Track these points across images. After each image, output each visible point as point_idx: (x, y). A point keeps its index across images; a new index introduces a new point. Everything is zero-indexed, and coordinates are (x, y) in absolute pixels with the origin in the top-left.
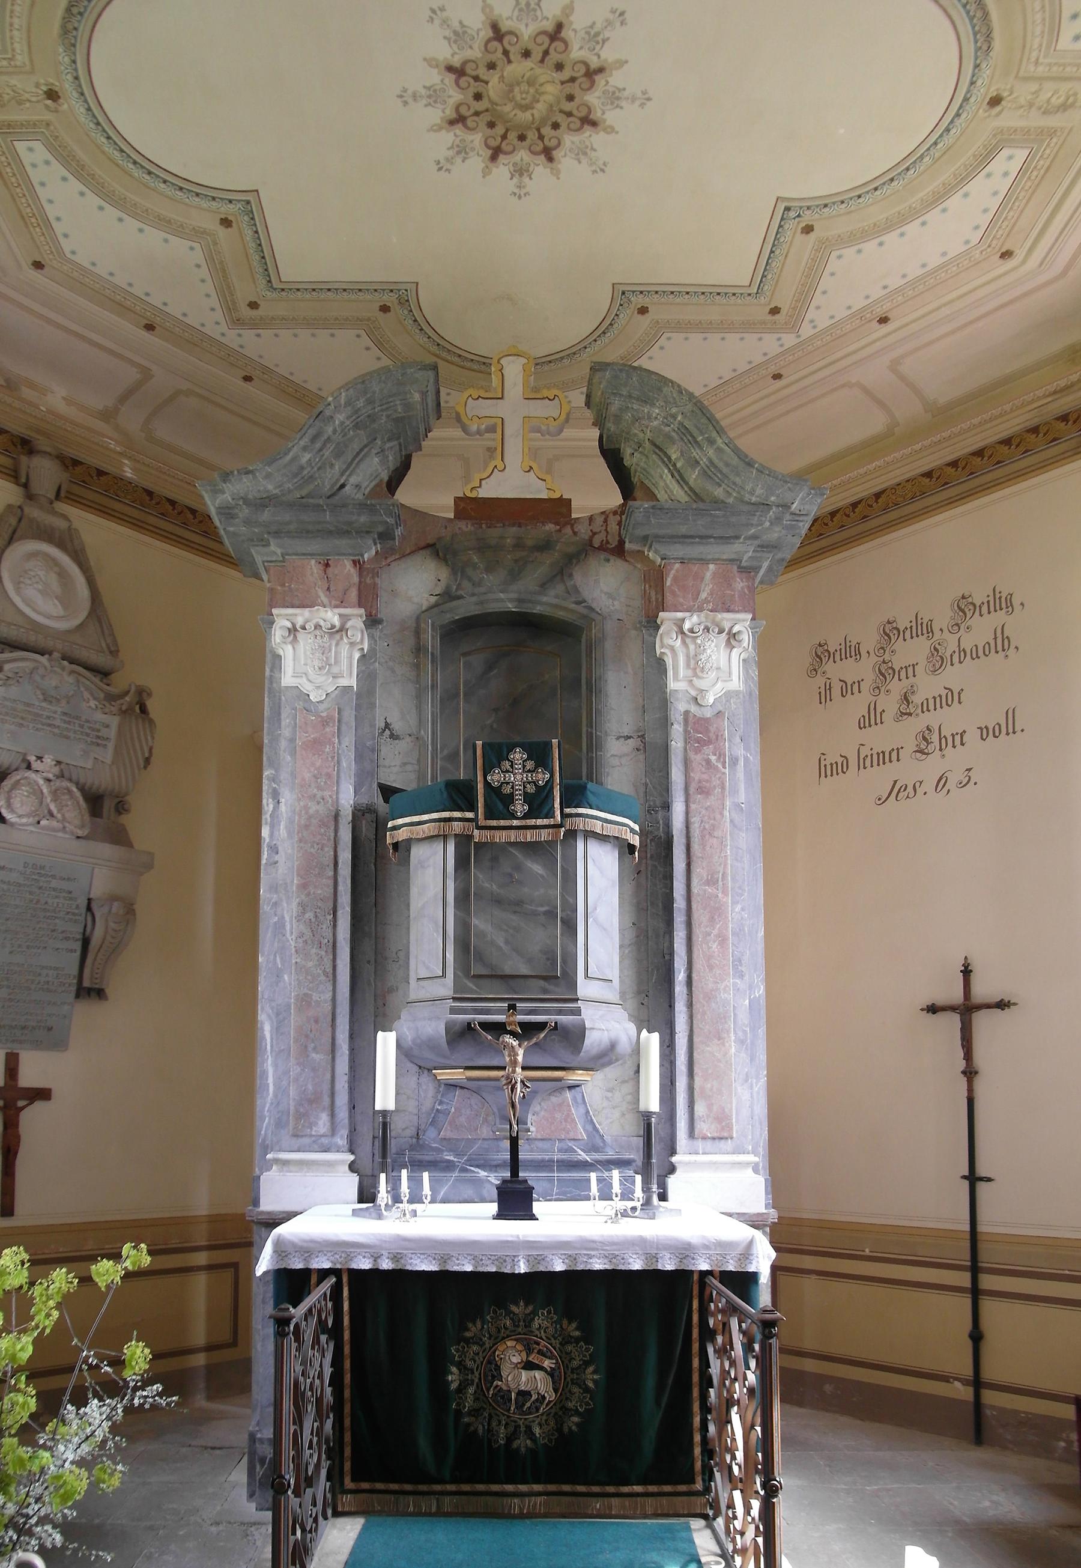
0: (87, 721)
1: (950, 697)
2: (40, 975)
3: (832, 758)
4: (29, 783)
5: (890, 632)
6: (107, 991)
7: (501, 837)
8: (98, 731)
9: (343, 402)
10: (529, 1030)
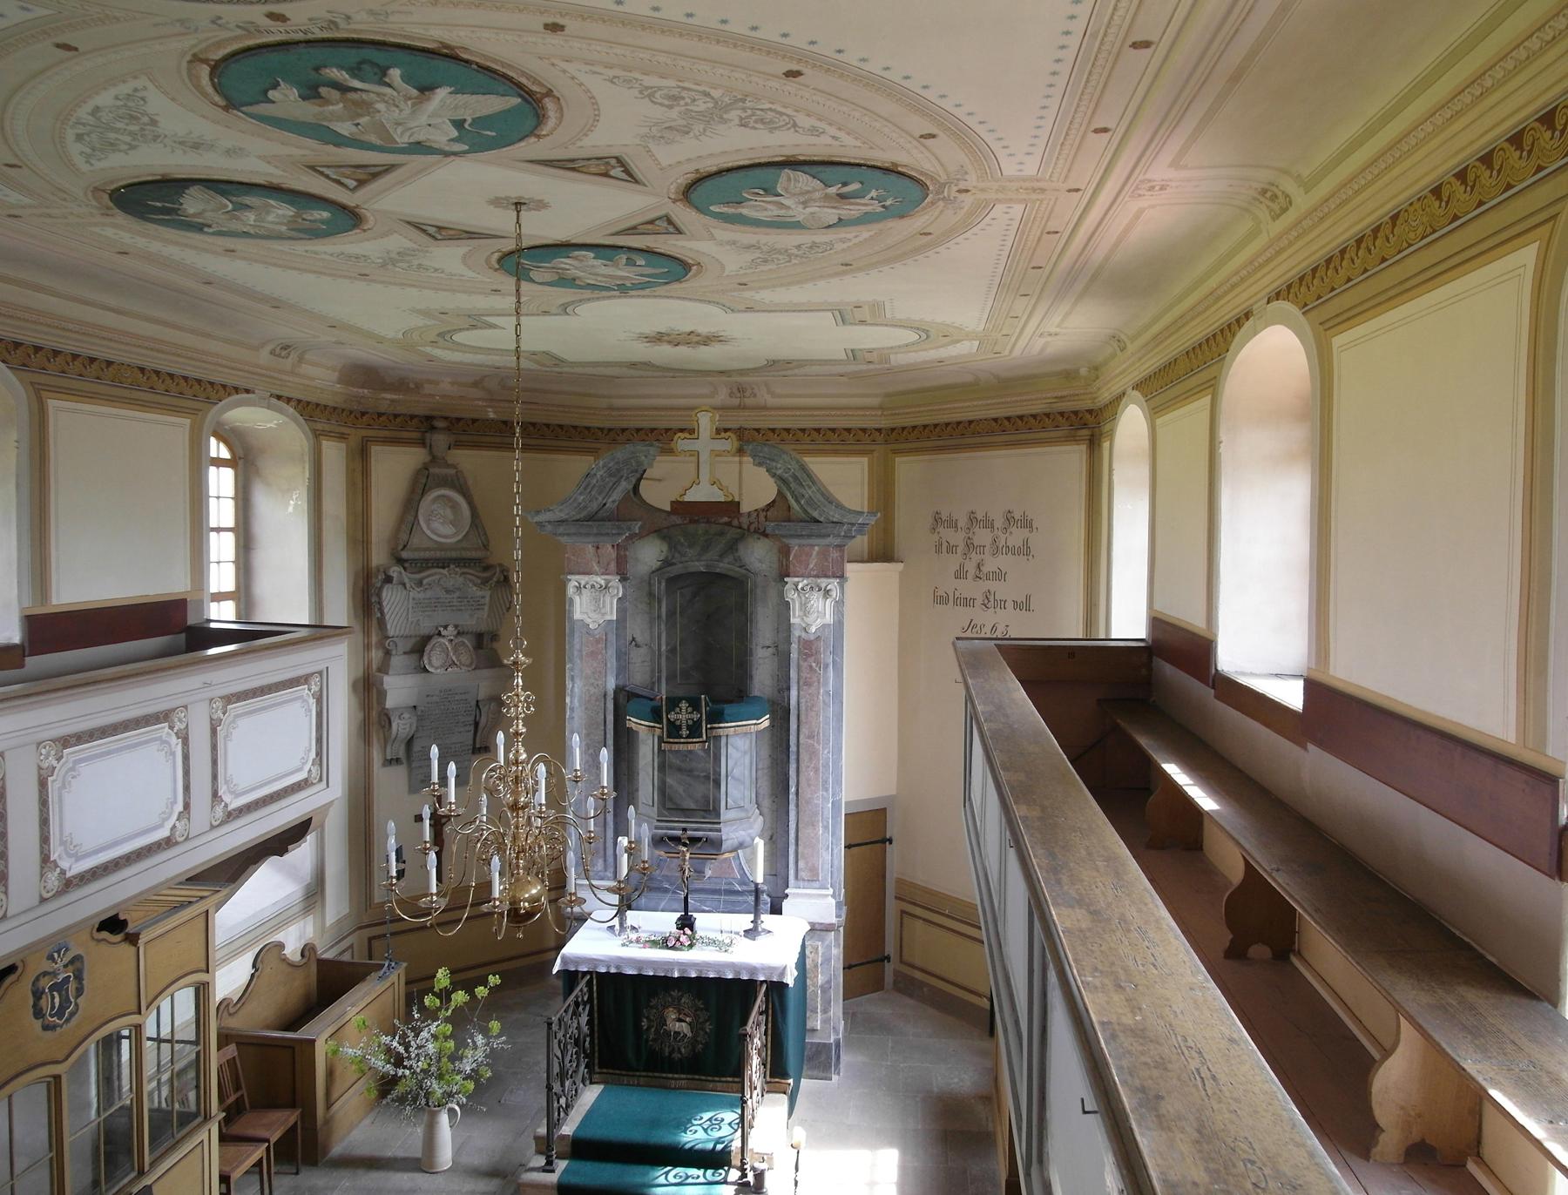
1: (1000, 575)
3: (940, 592)
5: (972, 518)
7: (676, 747)
10: (695, 840)
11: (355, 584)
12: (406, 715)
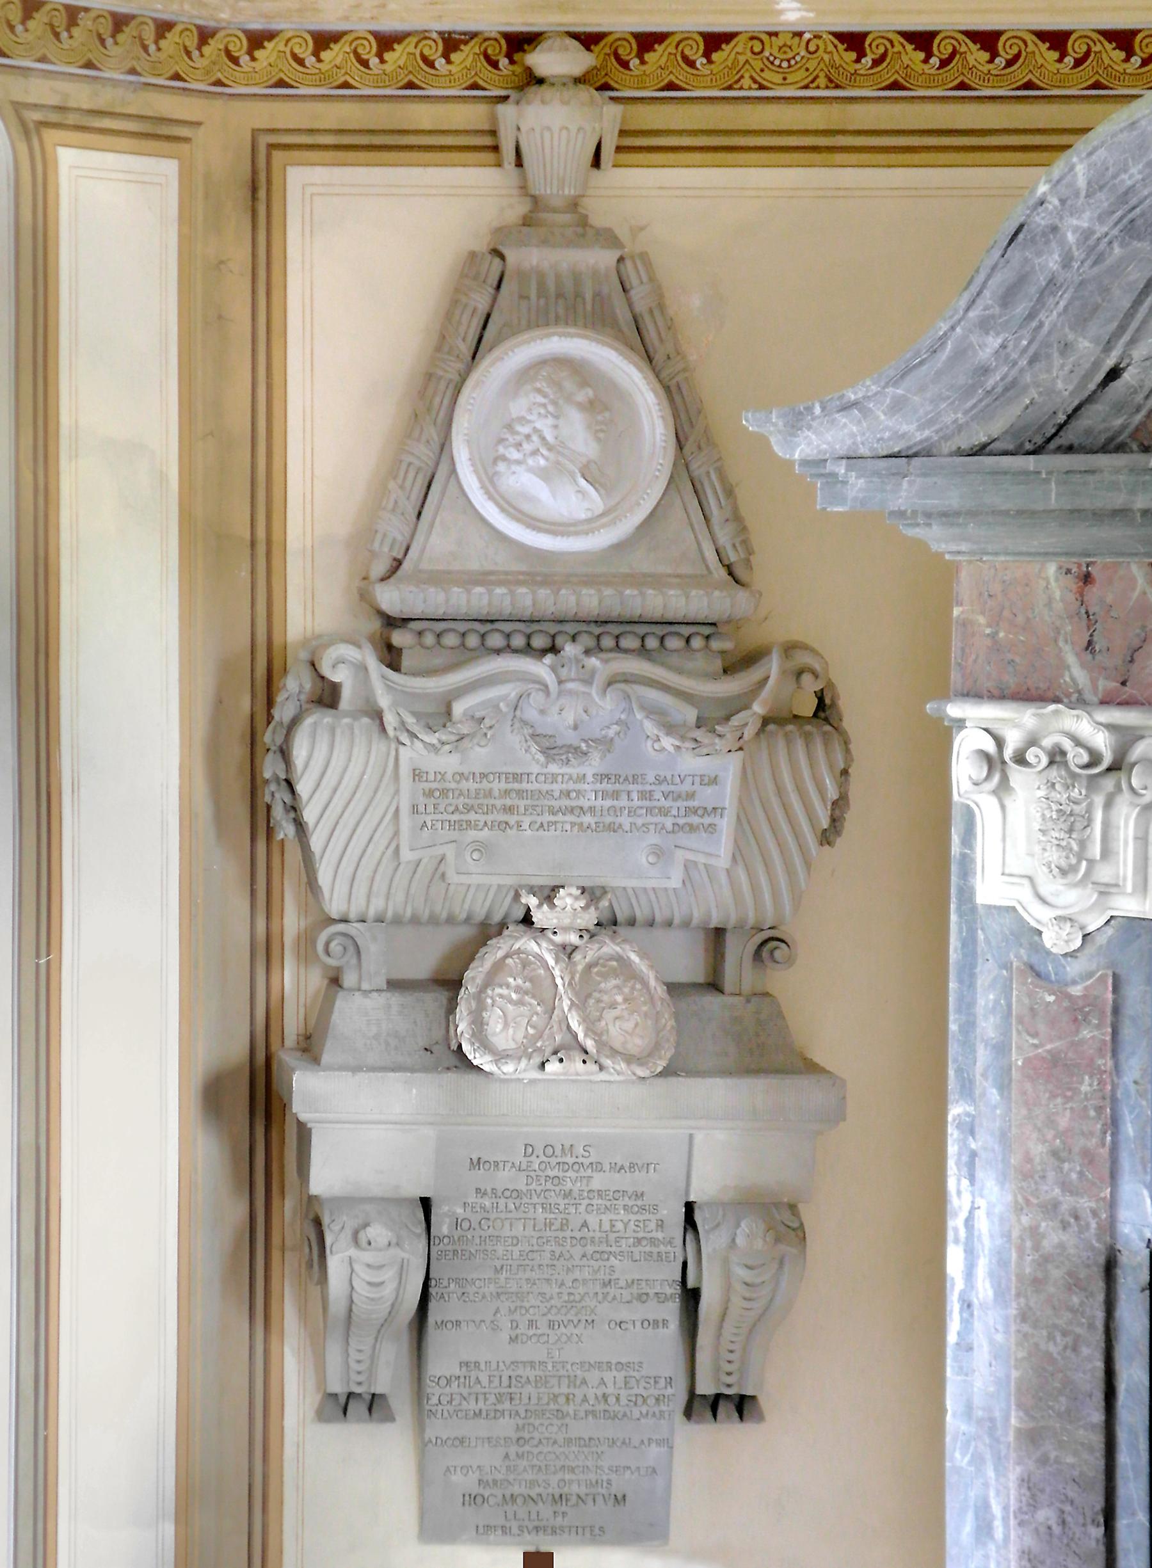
0: (660, 781)
2: (584, 1382)
4: (525, 964)
6: (762, 1401)
8: (691, 796)
9: (1081, 183)
11: (220, 705)
12: (378, 1232)
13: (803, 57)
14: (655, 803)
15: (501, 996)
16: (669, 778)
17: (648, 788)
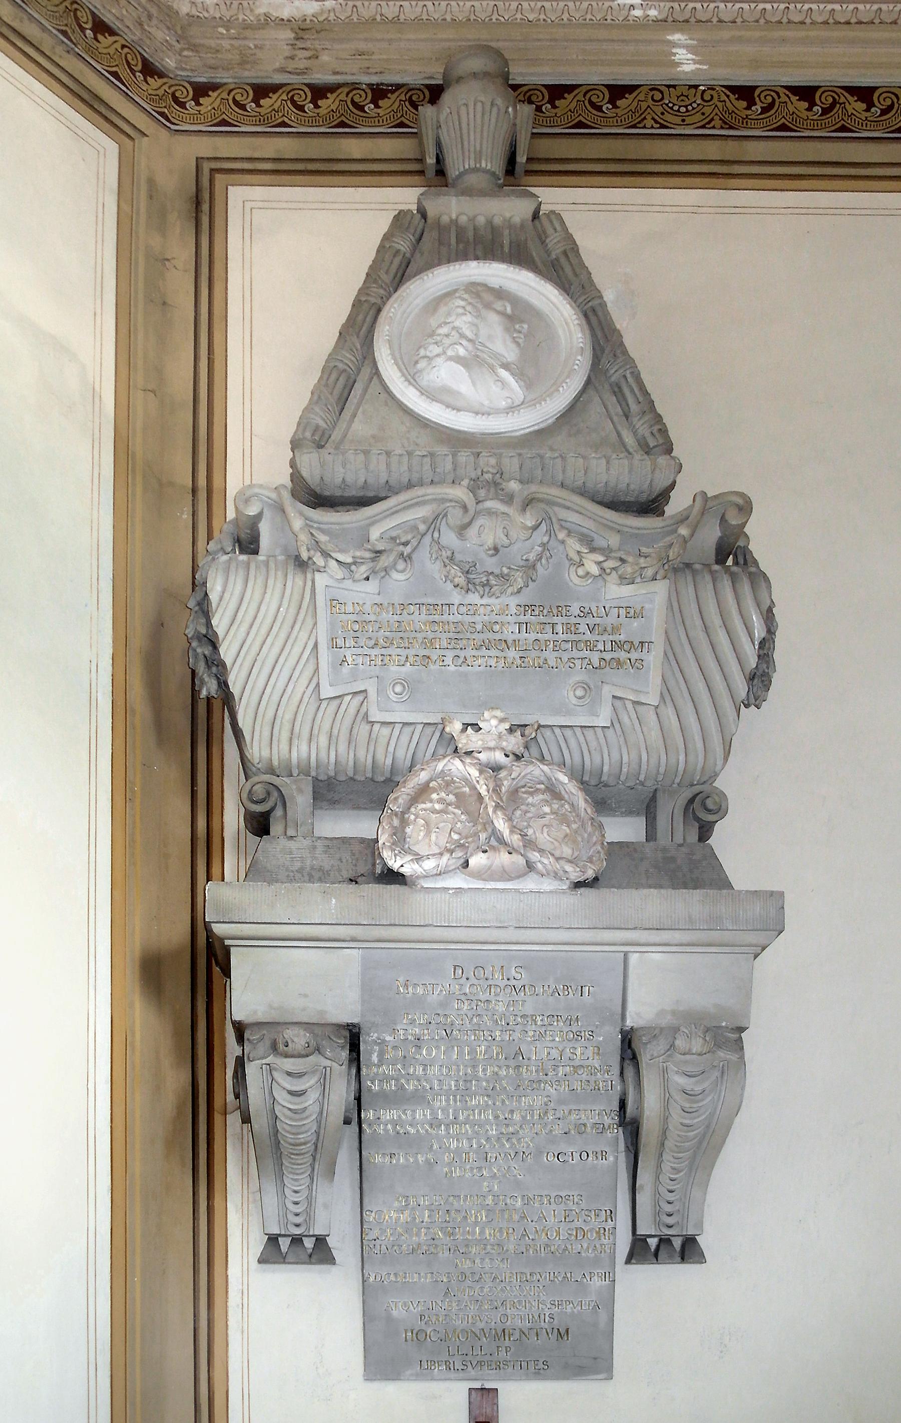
0: (585, 613)
8: (615, 629)
13: (698, 105)
14: (581, 637)
15: (422, 810)
16: (594, 610)
17: (573, 620)
